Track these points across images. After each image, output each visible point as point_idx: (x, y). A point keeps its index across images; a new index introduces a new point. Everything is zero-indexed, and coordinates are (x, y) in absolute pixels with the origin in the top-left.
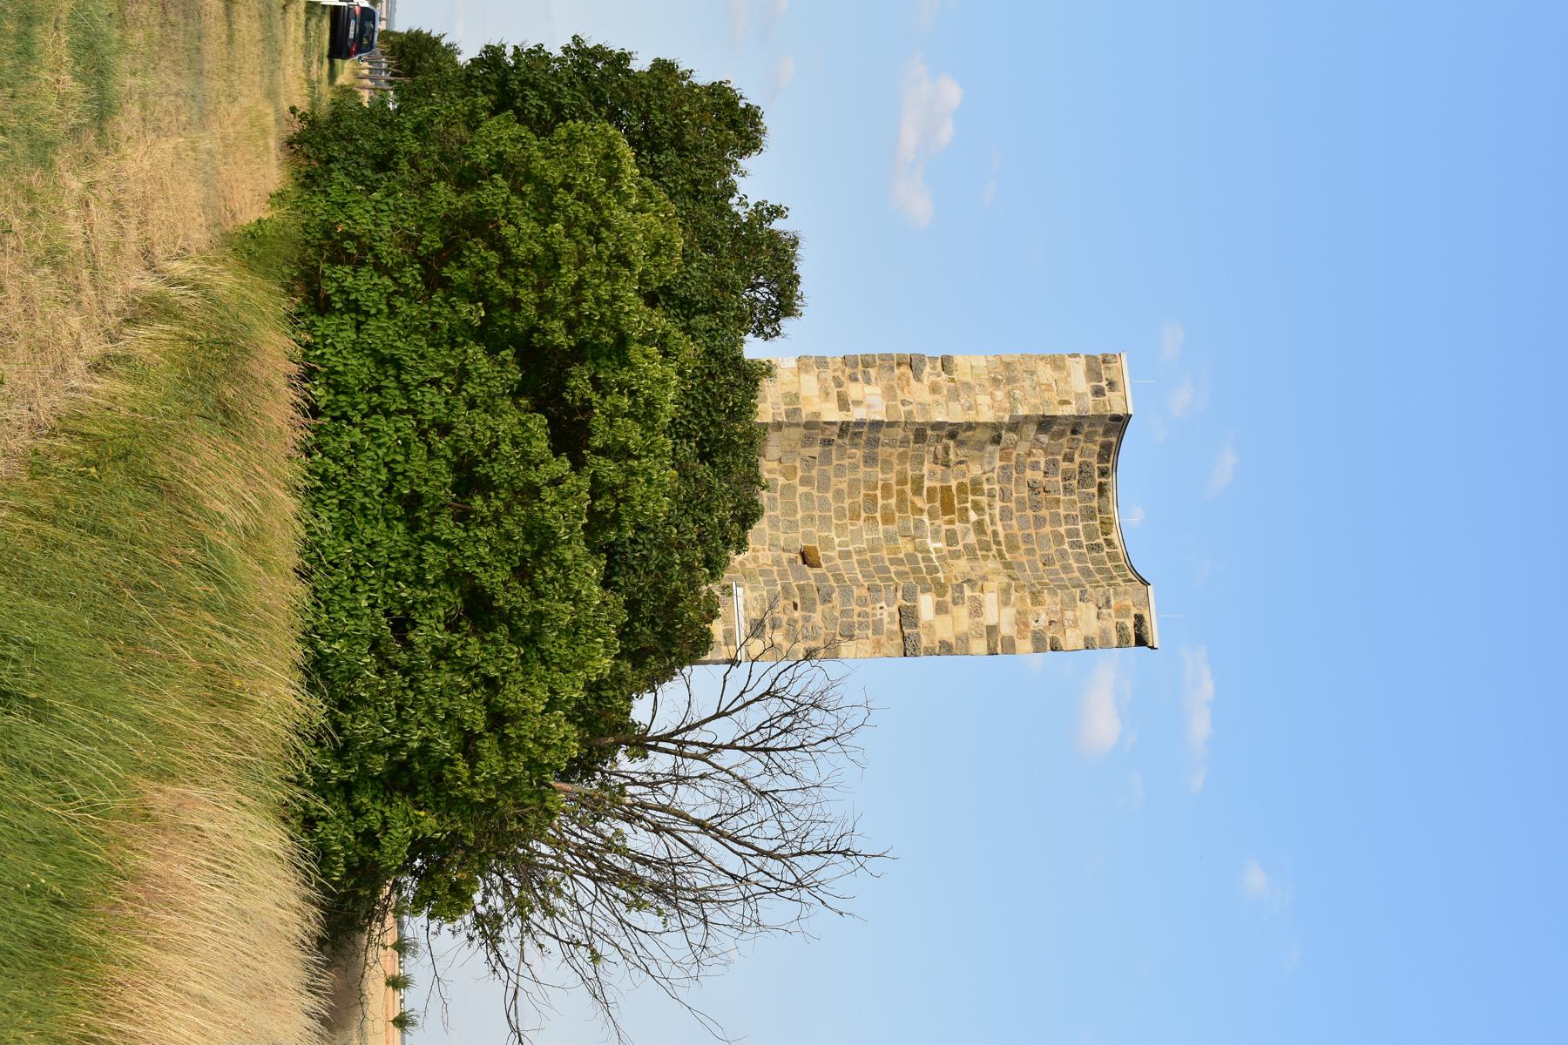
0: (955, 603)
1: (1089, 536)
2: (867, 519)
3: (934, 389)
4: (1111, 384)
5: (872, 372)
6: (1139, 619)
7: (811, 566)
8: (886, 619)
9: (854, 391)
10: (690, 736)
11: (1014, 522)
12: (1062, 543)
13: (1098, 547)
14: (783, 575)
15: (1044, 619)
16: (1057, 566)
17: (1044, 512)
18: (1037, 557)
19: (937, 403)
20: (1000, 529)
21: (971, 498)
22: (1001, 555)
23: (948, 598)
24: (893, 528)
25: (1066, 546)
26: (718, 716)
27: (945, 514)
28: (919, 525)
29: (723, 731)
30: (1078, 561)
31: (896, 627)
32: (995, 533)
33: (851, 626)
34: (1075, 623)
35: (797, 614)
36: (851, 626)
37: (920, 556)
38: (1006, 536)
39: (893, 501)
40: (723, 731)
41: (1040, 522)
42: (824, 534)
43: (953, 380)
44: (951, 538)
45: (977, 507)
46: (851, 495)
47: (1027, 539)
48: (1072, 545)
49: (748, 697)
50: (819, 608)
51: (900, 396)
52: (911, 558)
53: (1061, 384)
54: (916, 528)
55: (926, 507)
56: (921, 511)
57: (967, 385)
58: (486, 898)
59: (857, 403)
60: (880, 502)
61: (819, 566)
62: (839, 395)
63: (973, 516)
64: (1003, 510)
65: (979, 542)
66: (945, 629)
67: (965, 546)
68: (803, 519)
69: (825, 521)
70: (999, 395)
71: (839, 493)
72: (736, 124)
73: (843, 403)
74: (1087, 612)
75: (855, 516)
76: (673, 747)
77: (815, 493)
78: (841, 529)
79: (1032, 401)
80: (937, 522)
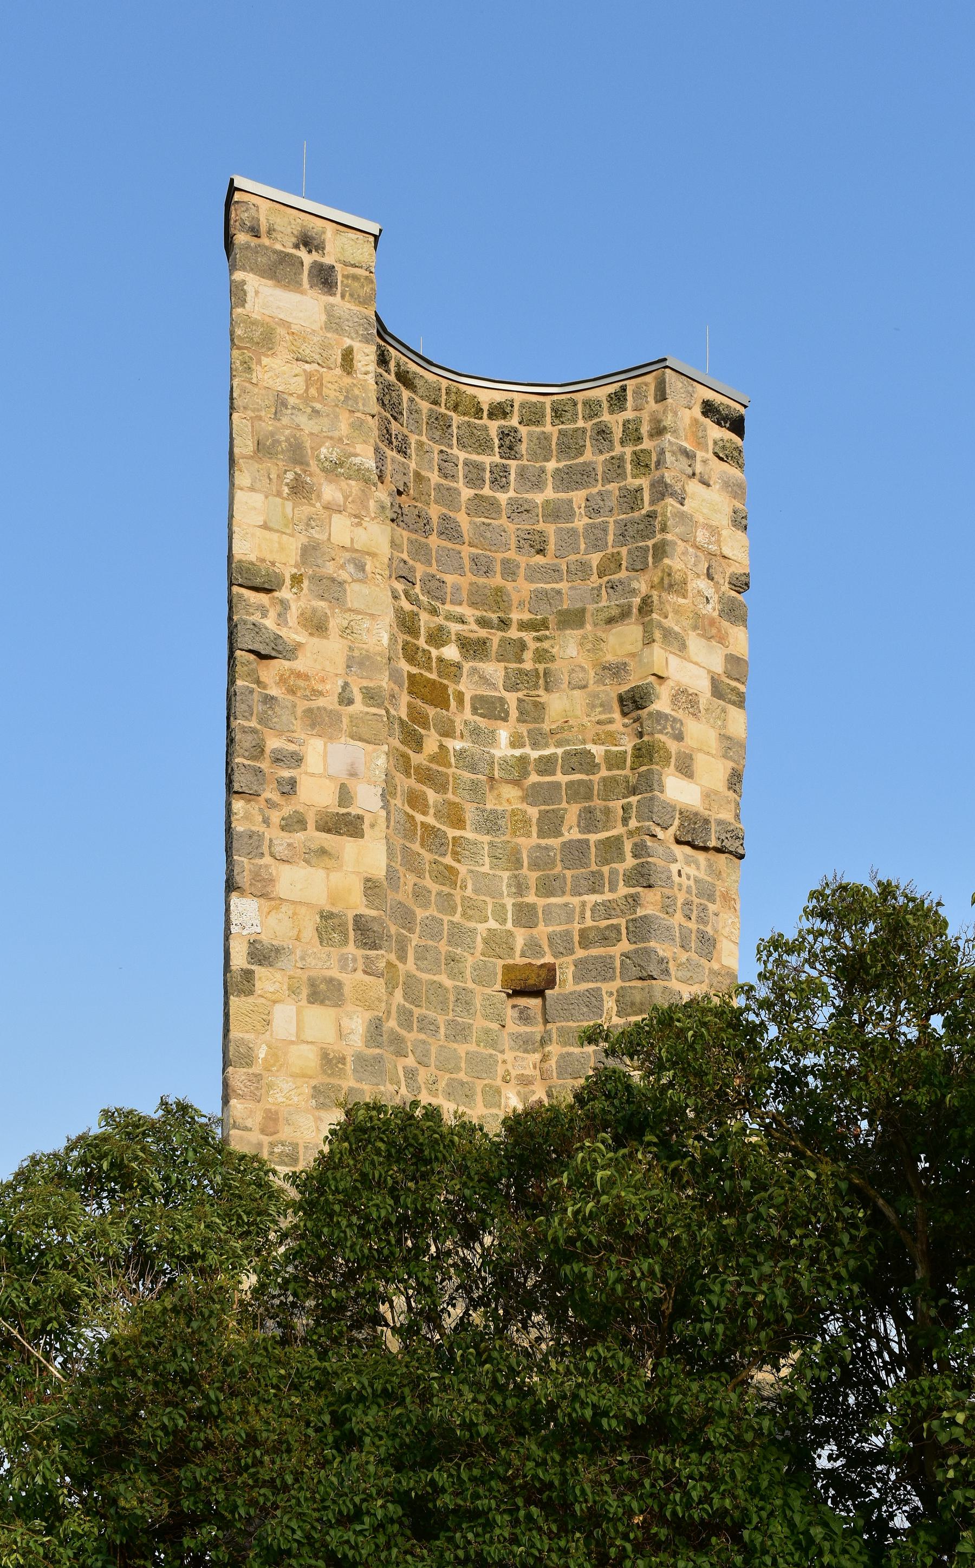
0: (679, 737)
1: (483, 446)
2: (456, 856)
3: (317, 625)
4: (307, 242)
5: (273, 743)
7: (551, 983)
9: (316, 794)
11: (450, 579)
12: (493, 504)
15: (703, 584)
16: (550, 529)
18: (522, 560)
19: (347, 631)
24: (470, 812)
25: (503, 497)
30: (538, 485)
37: (534, 778)
41: (449, 530)
42: (480, 945)
43: (297, 580)
44: (491, 709)
47: (482, 566)
51: (329, 702)
53: (307, 351)
54: (473, 768)
57: (309, 552)
59: (345, 796)
61: (550, 969)
65: (501, 658)
67: (511, 687)
68: (452, 976)
69: (458, 935)
70: (330, 492)
73: (346, 824)
75: (448, 876)
78: (472, 910)
79: (344, 428)
80: (459, 727)
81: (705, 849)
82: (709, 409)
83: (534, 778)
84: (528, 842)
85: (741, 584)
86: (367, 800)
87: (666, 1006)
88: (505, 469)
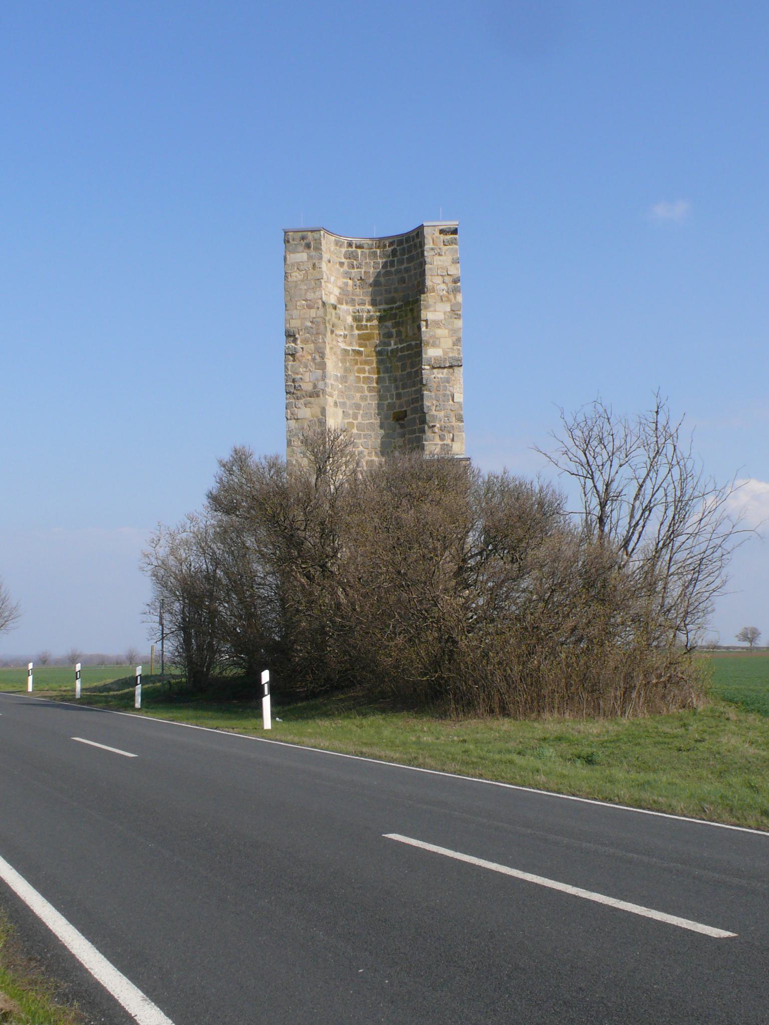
7: (406, 416)
9: (307, 387)
15: (443, 286)
21: (364, 323)
25: (393, 269)
35: (438, 425)
37: (400, 354)
38: (386, 303)
39: (367, 368)
59: (315, 386)
60: (367, 375)
67: (393, 328)
71: (362, 398)
77: (361, 412)
81: (445, 368)
82: (442, 232)
83: (400, 354)
84: (399, 373)
85: (456, 281)
88: (393, 261)
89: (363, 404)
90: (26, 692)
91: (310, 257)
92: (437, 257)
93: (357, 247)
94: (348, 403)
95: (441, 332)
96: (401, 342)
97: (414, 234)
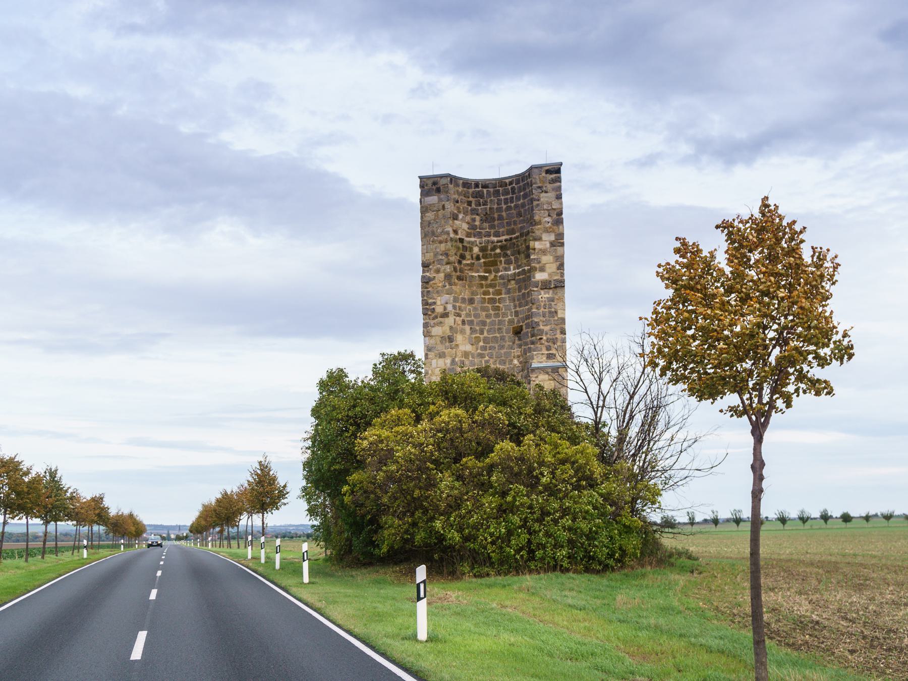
0: (539, 262)
1: (508, 193)
3: (438, 271)
5: (430, 301)
6: (548, 172)
8: (547, 296)
9: (439, 309)
10: (595, 403)
13: (513, 189)
14: (526, 344)
15: (548, 219)
17: (496, 216)
20: (504, 238)
21: (489, 252)
22: (517, 238)
23: (537, 266)
26: (586, 392)
27: (497, 265)
28: (502, 277)
29: (593, 389)
30: (505, 203)
31: (551, 291)
32: (506, 240)
33: (550, 312)
34: (550, 204)
35: (545, 338)
36: (550, 312)
38: (508, 234)
39: (491, 290)
40: (593, 389)
41: (500, 218)
45: (493, 249)
46: (488, 311)
47: (509, 224)
48: (512, 202)
49: (579, 380)
50: (542, 327)
52: (518, 282)
55: (494, 274)
56: (495, 276)
58: (657, 482)
59: (445, 309)
60: (491, 296)
62: (441, 317)
63: (498, 251)
64: (495, 236)
66: (552, 267)
71: (488, 316)
72: (334, 383)
74: (544, 198)
76: (600, 409)
77: (487, 328)
78: (504, 315)
80: (501, 268)
86: (450, 307)
87: (313, 419)
89: (488, 321)
90: (414, 637)
91: (440, 200)
92: (543, 195)
93: (483, 187)
94: (475, 321)
95: (545, 259)
96: (518, 267)
97: (507, 181)
